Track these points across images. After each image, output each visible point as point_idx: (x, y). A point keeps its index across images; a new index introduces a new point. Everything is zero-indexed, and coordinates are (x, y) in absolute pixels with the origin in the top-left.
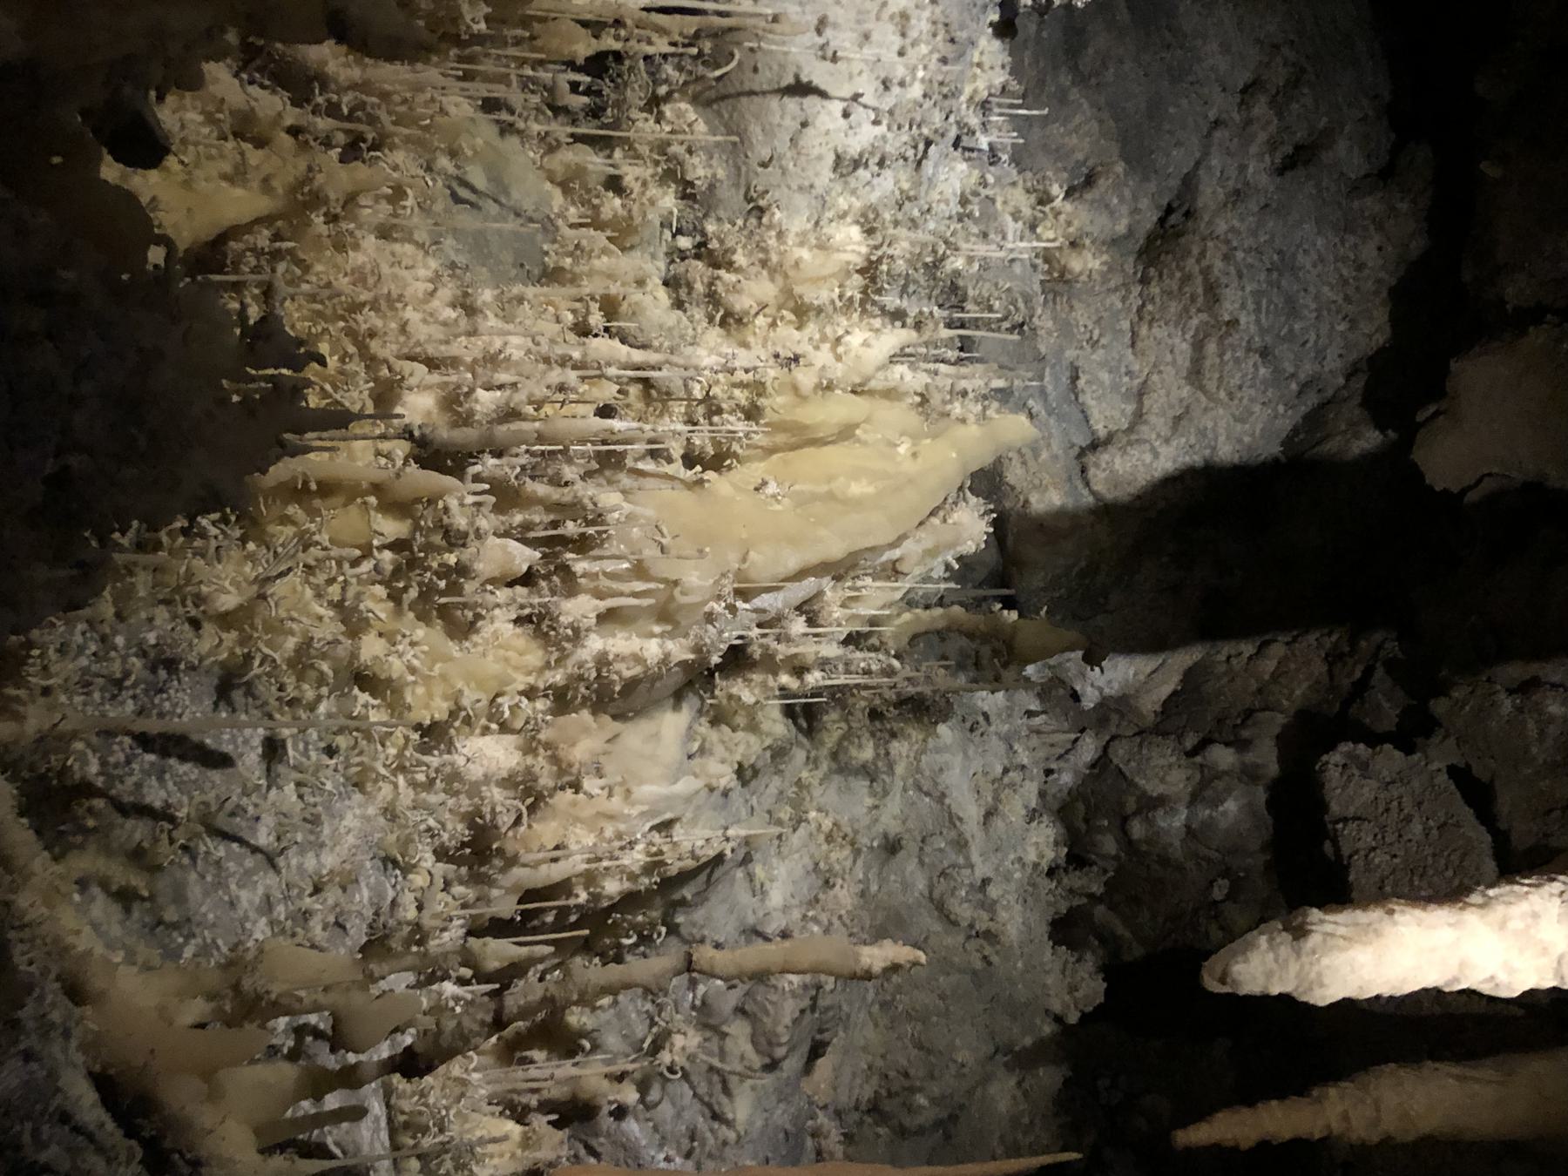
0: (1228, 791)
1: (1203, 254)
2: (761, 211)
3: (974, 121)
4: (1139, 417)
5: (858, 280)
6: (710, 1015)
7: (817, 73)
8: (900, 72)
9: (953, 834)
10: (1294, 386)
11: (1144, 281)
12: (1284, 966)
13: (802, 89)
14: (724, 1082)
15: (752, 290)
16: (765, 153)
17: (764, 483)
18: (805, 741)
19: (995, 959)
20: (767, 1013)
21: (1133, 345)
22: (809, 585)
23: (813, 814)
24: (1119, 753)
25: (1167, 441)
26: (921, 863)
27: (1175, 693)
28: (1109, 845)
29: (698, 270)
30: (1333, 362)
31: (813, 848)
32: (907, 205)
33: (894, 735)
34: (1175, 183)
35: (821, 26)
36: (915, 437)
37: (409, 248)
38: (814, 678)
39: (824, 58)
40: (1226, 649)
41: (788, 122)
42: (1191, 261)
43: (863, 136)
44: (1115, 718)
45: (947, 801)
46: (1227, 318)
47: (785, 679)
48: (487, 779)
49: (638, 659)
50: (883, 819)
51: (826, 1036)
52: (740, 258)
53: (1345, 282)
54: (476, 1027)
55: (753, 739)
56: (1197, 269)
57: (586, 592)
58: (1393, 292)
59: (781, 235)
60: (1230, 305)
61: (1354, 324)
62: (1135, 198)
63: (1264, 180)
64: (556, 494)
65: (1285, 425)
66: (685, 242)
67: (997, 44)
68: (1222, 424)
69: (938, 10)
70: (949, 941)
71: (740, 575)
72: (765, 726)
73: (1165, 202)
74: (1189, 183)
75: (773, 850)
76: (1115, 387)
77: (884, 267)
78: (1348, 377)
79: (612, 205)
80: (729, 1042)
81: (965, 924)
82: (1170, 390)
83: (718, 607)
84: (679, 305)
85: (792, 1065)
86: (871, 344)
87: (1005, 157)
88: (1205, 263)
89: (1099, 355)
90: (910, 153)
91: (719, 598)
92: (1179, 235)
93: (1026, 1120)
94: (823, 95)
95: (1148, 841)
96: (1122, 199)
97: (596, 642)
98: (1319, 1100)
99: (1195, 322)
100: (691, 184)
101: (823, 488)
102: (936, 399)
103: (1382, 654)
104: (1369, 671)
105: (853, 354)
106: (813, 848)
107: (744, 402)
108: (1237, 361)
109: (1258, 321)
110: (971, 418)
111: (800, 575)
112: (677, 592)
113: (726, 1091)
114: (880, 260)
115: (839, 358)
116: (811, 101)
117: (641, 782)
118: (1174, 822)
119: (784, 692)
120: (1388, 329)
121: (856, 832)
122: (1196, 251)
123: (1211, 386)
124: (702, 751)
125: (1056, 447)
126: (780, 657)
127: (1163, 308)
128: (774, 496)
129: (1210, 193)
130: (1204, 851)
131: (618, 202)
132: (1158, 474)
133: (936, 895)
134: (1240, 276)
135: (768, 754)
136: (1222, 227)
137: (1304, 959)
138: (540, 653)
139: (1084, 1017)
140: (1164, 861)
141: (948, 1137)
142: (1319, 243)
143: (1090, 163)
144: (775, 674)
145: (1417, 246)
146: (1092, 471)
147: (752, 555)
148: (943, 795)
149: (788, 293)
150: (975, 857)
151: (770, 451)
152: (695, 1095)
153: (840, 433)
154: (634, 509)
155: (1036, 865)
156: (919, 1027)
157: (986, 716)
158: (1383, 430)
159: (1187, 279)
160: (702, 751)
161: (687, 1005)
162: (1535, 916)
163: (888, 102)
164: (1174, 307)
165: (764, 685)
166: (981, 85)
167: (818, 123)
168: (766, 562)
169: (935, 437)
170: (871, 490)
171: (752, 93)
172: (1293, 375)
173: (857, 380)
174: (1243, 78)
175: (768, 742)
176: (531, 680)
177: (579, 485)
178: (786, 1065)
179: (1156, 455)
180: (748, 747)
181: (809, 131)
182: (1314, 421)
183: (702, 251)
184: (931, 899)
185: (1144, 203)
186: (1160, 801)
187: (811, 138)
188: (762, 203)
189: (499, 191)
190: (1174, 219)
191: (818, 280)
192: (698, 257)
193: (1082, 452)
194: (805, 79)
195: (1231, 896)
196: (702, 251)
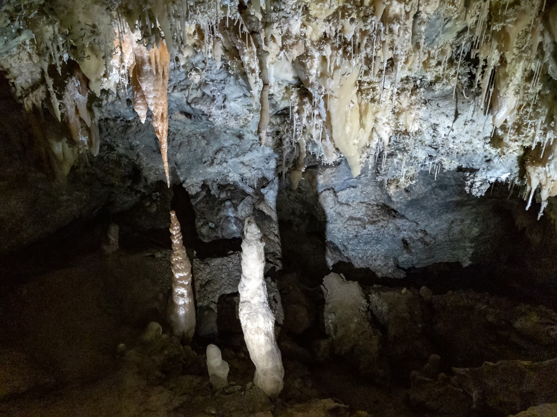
0: (239, 227)
1: (384, 220)
2: (425, 103)
3: (436, 161)
4: (341, 204)
5: (404, 129)
6: (204, 85)
7: (461, 119)
8: (457, 141)
9: (240, 154)
10: (346, 244)
11: (377, 205)
12: (254, 236)
13: (457, 115)
14: (184, 89)
15: (405, 101)
16: (441, 105)
17: (353, 103)
18: (275, 113)
19: (206, 165)
20: (204, 102)
21: (361, 202)
22: (324, 115)
23: (252, 115)
24: (248, 199)
25: (335, 211)
26: (232, 145)
27: (264, 213)
28: (223, 196)
29: (411, 86)
30: (351, 253)
31: (243, 115)
32: (420, 143)
33: (273, 138)
34: (403, 213)
35: (473, 121)
36: (358, 145)
37: (437, 6)
38: (296, 116)
39: (466, 122)
40: (276, 227)
41: (448, 111)
42: (382, 217)
43: (442, 131)
44: (258, 197)
45: (249, 152)
46: (366, 226)
47: (296, 108)
48: (290, 25)
49: (311, 67)
50: (248, 134)
51: (193, 118)
52: (413, 98)
53: (372, 256)
54: (253, 26)
55: (280, 98)
56: (380, 219)
57: (332, 53)
58: (368, 268)
59: (419, 109)
60: (370, 227)
61: (361, 259)
62: (401, 203)
63: (401, 236)
64: (363, 46)
65: (336, 242)
66: (418, 82)
67: (456, 167)
68: (338, 226)
69: (471, 152)
70: (211, 152)
71: (331, 96)
72: (283, 102)
73: (398, 210)
74: (403, 217)
75: (244, 104)
76: (350, 198)
77: (407, 137)
78: (347, 257)
79: (433, 62)
80: (195, 91)
81: (216, 156)
82: (347, 212)
83: (323, 90)
84: (402, 80)
85: (188, 109)
86: (385, 133)
87: (422, 168)
88: (381, 221)
89: (359, 193)
90: (435, 144)
91: (326, 90)
92: (389, 215)
93: (157, 173)
94: (454, 121)
95: (224, 206)
96: (401, 199)
97: (317, 55)
98: (182, 248)
99: (366, 218)
100: (434, 85)
101: (349, 120)
102: (368, 150)
103: (276, 266)
104: (272, 263)
105: (384, 128)
106: (243, 115)
107: (376, 97)
108: (354, 229)
109: (364, 234)
110: (361, 160)
111: (328, 113)
112: (330, 78)
113: (182, 90)
114: (409, 135)
115: (384, 124)
116: (453, 118)
117: (275, 67)
118: (230, 213)
119: (293, 108)
120: (359, 267)
121: (248, 127)
122: (385, 218)
123: (348, 223)
124: (279, 84)
125: (335, 182)
126: (304, 106)
127: (370, 210)
128: (349, 106)
129: (399, 222)
130: (222, 221)
131: (434, 64)
132: (326, 209)
133: (224, 149)
134: (377, 230)
135: (275, 103)
136: (390, 225)
137: (255, 242)
138: (316, 39)
139: (184, 189)
140: (219, 210)
141: (154, 151)
142: (383, 250)
143: (412, 191)
144: (298, 105)
145: (379, 275)
146: (328, 192)
147: (336, 100)
148: (251, 151)
149: (403, 111)
150: (233, 160)
151: (360, 105)
152: (180, 81)
153: (363, 124)
154: (354, 68)
155: (228, 176)
156: (187, 143)
157: (268, 163)
158: (332, 266)
159: (377, 216)
160: (279, 84)
161: (206, 79)
162: (260, 296)
163: (450, 138)
164: (370, 213)
165: (295, 102)
166: (446, 163)
167: (447, 119)
168: (333, 105)
169: (358, 150)
170: (347, 132)
171: (457, 102)
172: (349, 243)
173: (377, 129)
174: (428, 230)
175: (278, 103)
176: (308, 37)
177: (365, 52)
178: (188, 107)
179: (331, 208)
180: (278, 98)
181: (445, 117)
182: (336, 249)
183: (416, 87)
184: (223, 147)
185: (399, 205)
186: (236, 210)
187: (443, 117)
188: (427, 104)
189: (445, 31)
190: (393, 213)
191: (406, 119)
192: (414, 86)
193: (333, 189)
194: (459, 116)
195: (210, 228)
196: (416, 87)
